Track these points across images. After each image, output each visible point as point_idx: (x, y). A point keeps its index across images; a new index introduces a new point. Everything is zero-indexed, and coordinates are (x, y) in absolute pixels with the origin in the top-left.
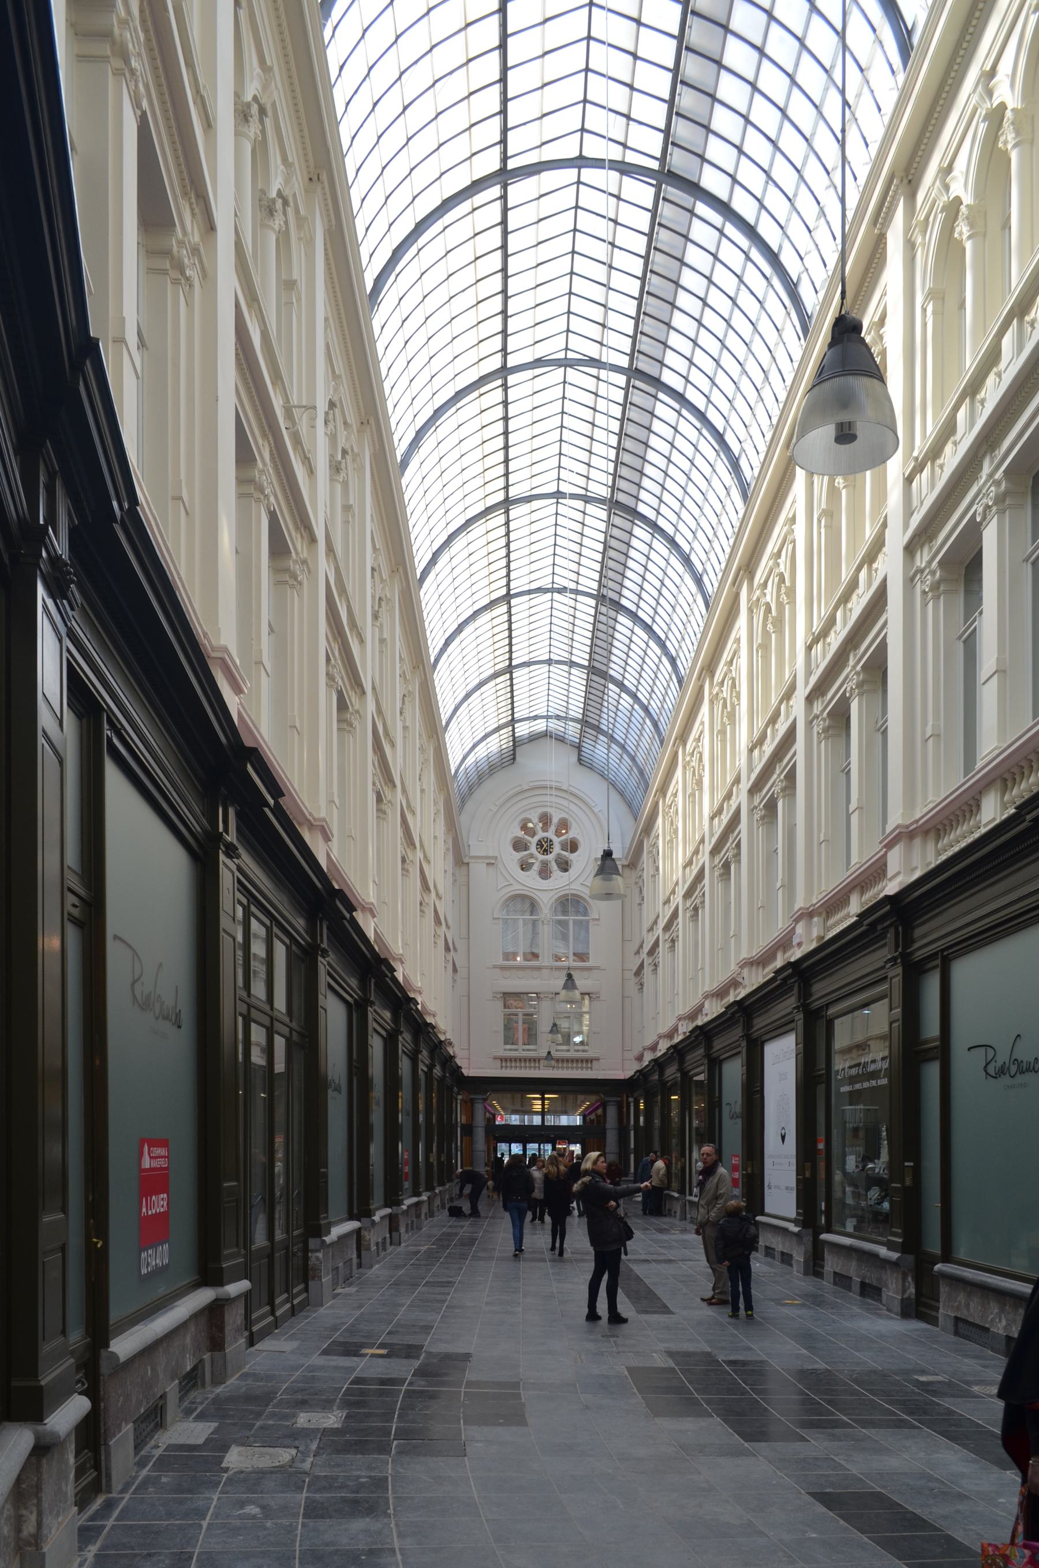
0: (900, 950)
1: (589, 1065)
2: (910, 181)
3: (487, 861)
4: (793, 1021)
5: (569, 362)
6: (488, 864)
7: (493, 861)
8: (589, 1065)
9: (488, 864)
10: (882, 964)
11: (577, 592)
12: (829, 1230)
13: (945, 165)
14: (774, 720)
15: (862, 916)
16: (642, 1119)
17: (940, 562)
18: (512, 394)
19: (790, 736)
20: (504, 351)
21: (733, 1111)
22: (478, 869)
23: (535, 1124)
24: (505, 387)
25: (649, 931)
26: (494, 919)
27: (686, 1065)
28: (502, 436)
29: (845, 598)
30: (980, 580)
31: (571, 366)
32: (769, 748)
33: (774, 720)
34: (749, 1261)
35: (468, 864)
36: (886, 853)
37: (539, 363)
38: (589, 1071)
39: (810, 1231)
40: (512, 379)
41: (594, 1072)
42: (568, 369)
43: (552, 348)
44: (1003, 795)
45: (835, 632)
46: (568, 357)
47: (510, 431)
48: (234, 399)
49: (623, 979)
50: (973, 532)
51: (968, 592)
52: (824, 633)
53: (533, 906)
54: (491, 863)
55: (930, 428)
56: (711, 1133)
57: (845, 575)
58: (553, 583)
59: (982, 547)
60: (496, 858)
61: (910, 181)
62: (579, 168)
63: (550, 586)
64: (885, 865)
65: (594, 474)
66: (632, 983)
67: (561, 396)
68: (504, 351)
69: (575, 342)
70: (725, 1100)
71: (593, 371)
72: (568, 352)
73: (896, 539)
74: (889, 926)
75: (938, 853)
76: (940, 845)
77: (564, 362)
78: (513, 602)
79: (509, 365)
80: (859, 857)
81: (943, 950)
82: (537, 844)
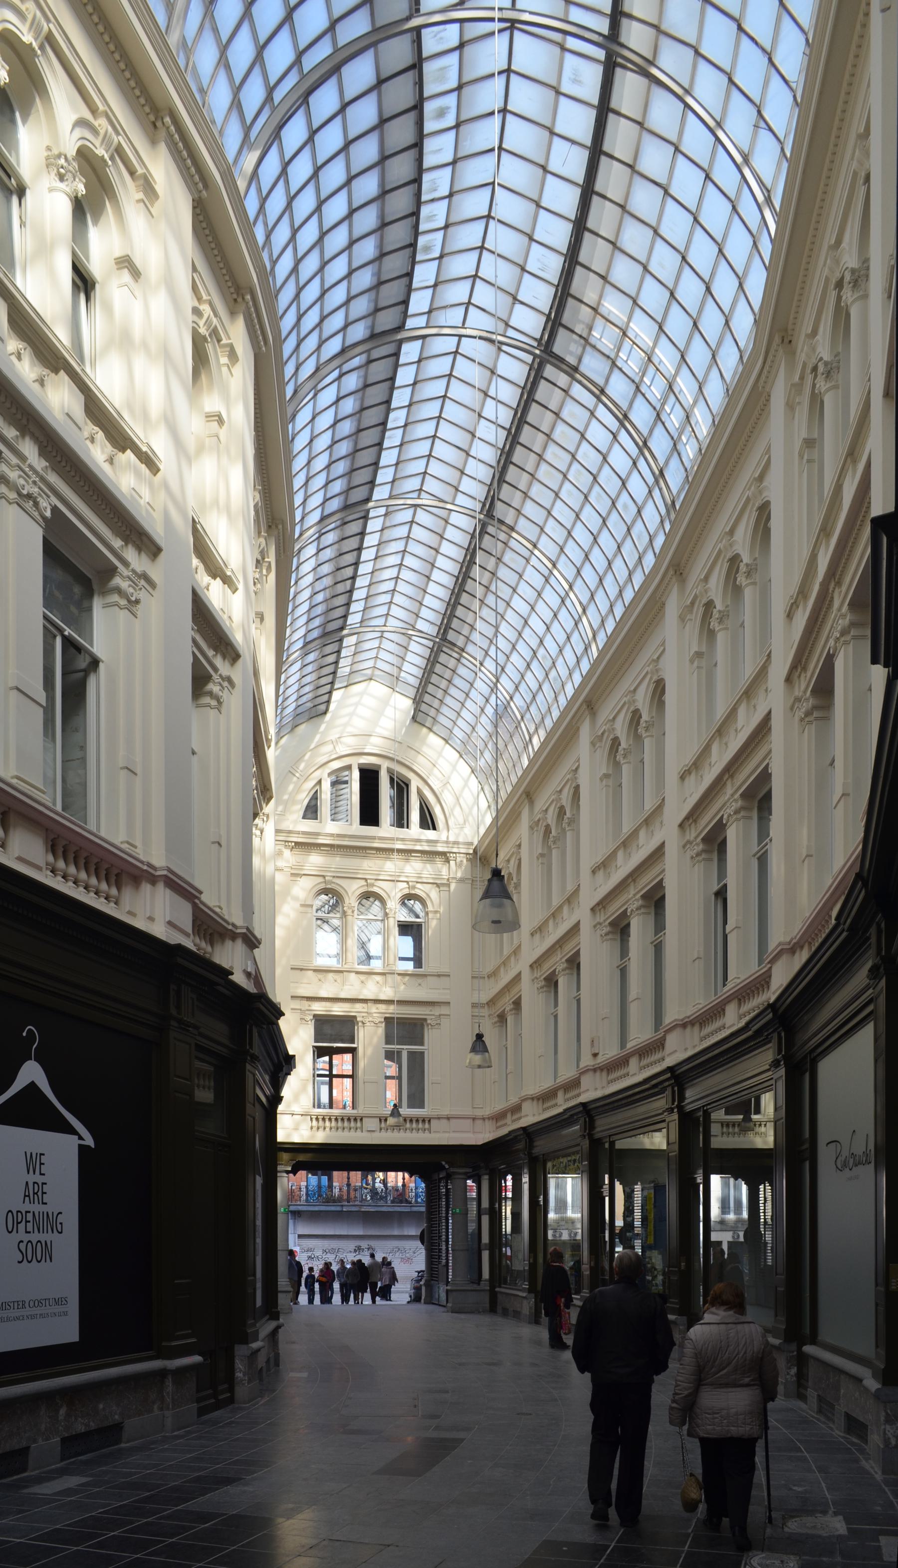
0: (676, 1103)
1: (427, 1126)
4: (664, 1121)
8: (427, 1126)
10: (661, 1111)
14: (555, 915)
15: (566, 1111)
16: (607, 1182)
17: (741, 795)
21: (845, 1153)
23: (359, 1173)
27: (687, 1101)
29: (720, 732)
30: (726, 860)
32: (735, 743)
34: (667, 1361)
36: (770, 968)
38: (427, 1134)
39: (685, 1318)
41: (433, 1135)
44: (640, 1060)
45: (736, 730)
50: (720, 827)
51: (656, 914)
56: (440, 1257)
57: (721, 711)
59: (726, 838)
64: (770, 977)
70: (823, 1137)
74: (669, 1086)
75: (702, 1039)
76: (641, 1064)
80: (567, 1073)
81: (704, 1106)
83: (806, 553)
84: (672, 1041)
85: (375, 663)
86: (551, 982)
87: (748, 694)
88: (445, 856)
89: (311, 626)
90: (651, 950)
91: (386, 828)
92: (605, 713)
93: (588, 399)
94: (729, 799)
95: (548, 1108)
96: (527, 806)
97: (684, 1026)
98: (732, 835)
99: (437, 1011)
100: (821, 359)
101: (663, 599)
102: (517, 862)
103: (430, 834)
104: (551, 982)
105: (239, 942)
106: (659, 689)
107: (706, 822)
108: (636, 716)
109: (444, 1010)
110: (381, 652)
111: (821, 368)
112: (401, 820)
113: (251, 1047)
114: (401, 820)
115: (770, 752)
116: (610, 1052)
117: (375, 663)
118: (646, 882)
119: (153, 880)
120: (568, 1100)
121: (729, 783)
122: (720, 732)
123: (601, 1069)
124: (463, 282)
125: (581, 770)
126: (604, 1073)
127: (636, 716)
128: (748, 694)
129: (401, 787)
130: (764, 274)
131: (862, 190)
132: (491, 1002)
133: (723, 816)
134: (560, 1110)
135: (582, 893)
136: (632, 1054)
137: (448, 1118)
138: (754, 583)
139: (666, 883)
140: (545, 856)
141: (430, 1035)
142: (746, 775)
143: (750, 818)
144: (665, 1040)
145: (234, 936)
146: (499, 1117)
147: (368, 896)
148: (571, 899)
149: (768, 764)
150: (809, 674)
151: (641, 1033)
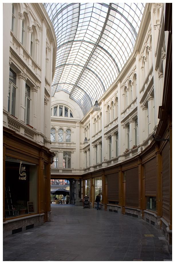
14: (97, 134)
48: (44, 97)
83: (142, 85)
84: (120, 159)
87: (133, 103)
88: (75, 122)
91: (63, 117)
95: (100, 167)
97: (122, 156)
99: (73, 150)
100: (148, 46)
103: (72, 118)
105: (49, 143)
106: (117, 98)
108: (112, 102)
109: (75, 150)
111: (148, 48)
112: (66, 115)
113: (42, 156)
114: (66, 115)
115: (153, 86)
116: (108, 159)
118: (115, 130)
119: (38, 135)
120: (133, 155)
121: (130, 117)
122: (128, 108)
123: (106, 163)
126: (107, 163)
128: (133, 103)
129: (66, 110)
130: (144, 8)
131: (150, 37)
132: (84, 149)
135: (102, 131)
136: (112, 160)
137: (75, 170)
138: (134, 85)
139: (119, 131)
141: (72, 155)
143: (133, 122)
144: (138, 149)
145: (48, 142)
146: (85, 170)
147: (61, 129)
150: (144, 102)
151: (114, 156)
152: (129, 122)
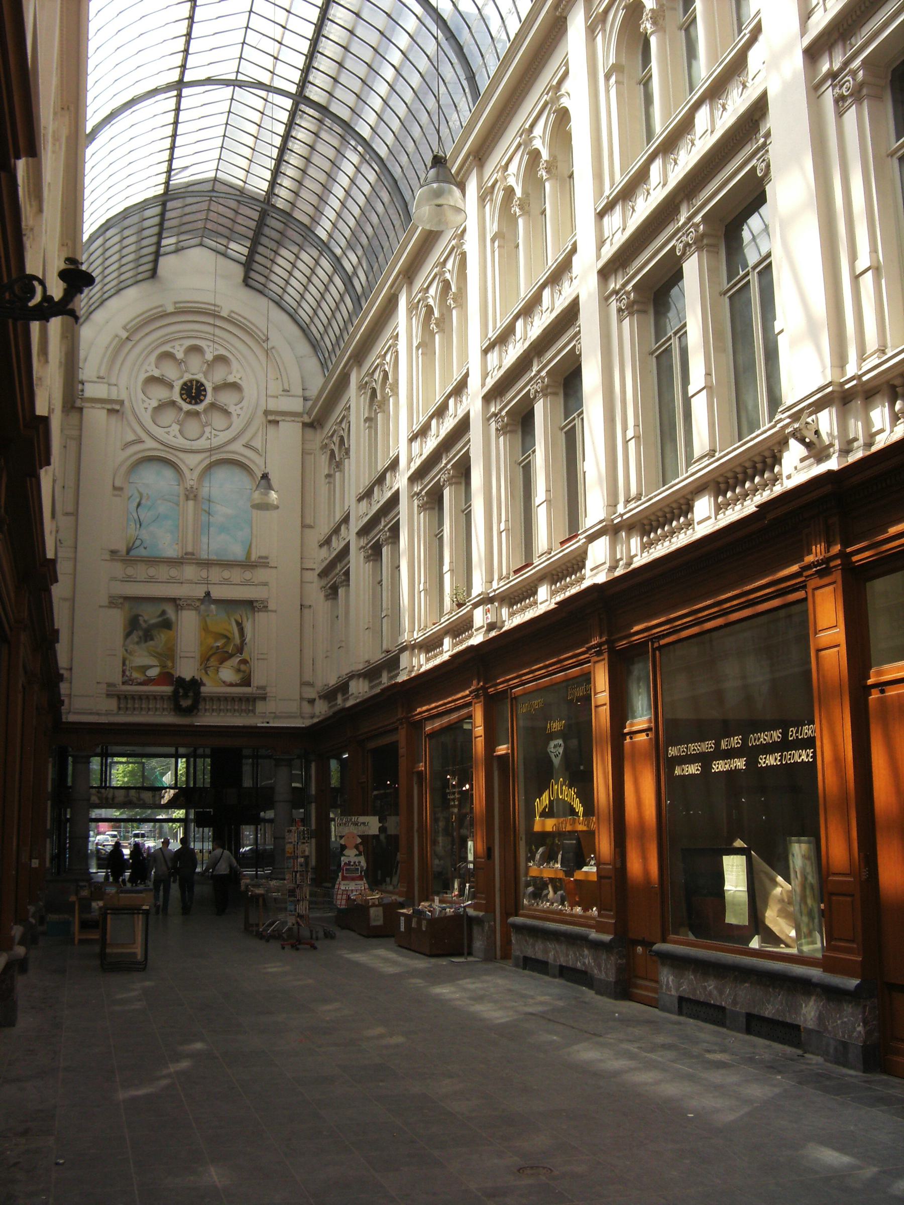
2: (480, 159)
3: (109, 407)
5: (239, 83)
6: (110, 411)
7: (117, 407)
9: (110, 411)
11: (269, 88)
12: (664, 940)
13: (601, 11)
14: (441, 412)
18: (184, 104)
19: (463, 426)
20: (183, 67)
22: (96, 417)
24: (179, 97)
25: (360, 500)
26: (115, 488)
28: (173, 112)
31: (240, 87)
33: (441, 412)
35: (81, 409)
37: (209, 81)
40: (185, 92)
42: (237, 88)
43: (227, 70)
46: (238, 79)
47: (181, 108)
49: (302, 582)
51: (567, 396)
52: (627, 194)
53: (173, 403)
54: (115, 409)
55: (421, 419)
58: (238, 72)
60: (122, 403)
61: (480, 159)
62: (236, 80)
63: (233, 77)
65: (255, 169)
66: (315, 593)
67: (236, 70)
68: (183, 67)
69: (246, 68)
71: (263, 94)
72: (239, 74)
73: (476, 390)
77: (236, 83)
78: (185, 92)
79: (185, 80)
82: (182, 389)
85: (205, 224)
86: (434, 501)
87: (336, 531)
89: (124, 261)
90: (562, 438)
92: (420, 281)
93: (335, 108)
94: (535, 375)
96: (475, 170)
98: (539, 408)
101: (564, 15)
102: (348, 425)
104: (434, 501)
107: (513, 397)
110: (211, 214)
117: (205, 224)
124: (171, 208)
125: (466, 237)
127: (447, 285)
133: (530, 390)
134: (446, 657)
140: (426, 345)
142: (554, 356)
148: (460, 388)
149: (469, 448)
150: (328, 579)
152: (532, 391)
